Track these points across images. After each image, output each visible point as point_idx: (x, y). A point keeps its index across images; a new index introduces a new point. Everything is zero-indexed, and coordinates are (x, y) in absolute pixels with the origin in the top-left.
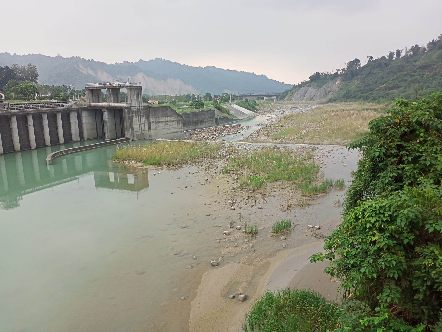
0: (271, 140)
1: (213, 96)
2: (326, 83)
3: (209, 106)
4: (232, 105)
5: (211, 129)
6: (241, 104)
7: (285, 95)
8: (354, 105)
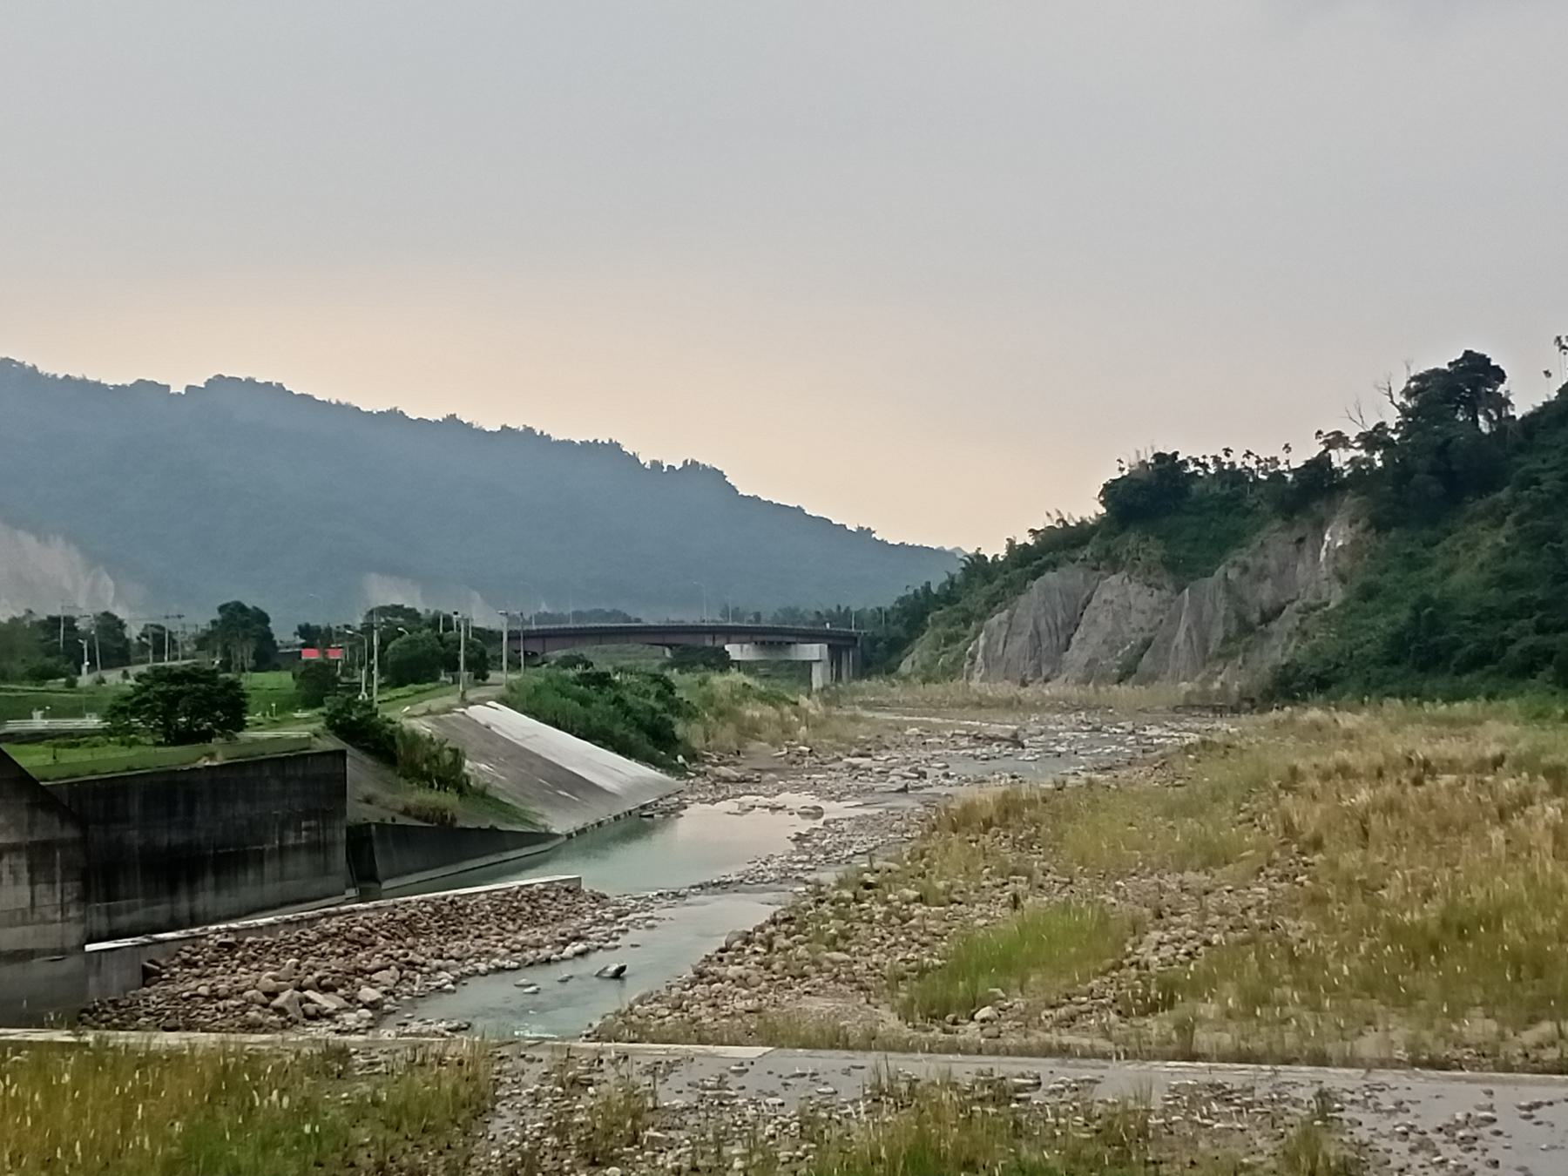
0: (889, 1021)
1: (284, 633)
2: (1236, 539)
3: (282, 727)
4: (476, 712)
5: (332, 925)
6: (552, 700)
7: (898, 630)
8: (1494, 728)
